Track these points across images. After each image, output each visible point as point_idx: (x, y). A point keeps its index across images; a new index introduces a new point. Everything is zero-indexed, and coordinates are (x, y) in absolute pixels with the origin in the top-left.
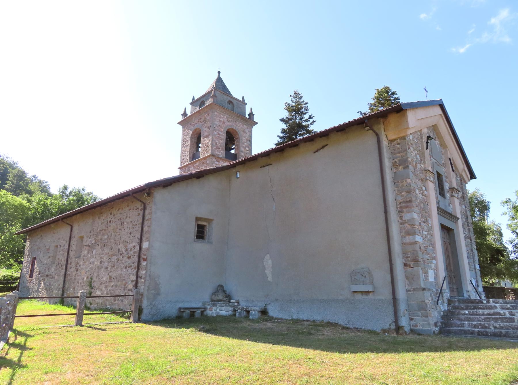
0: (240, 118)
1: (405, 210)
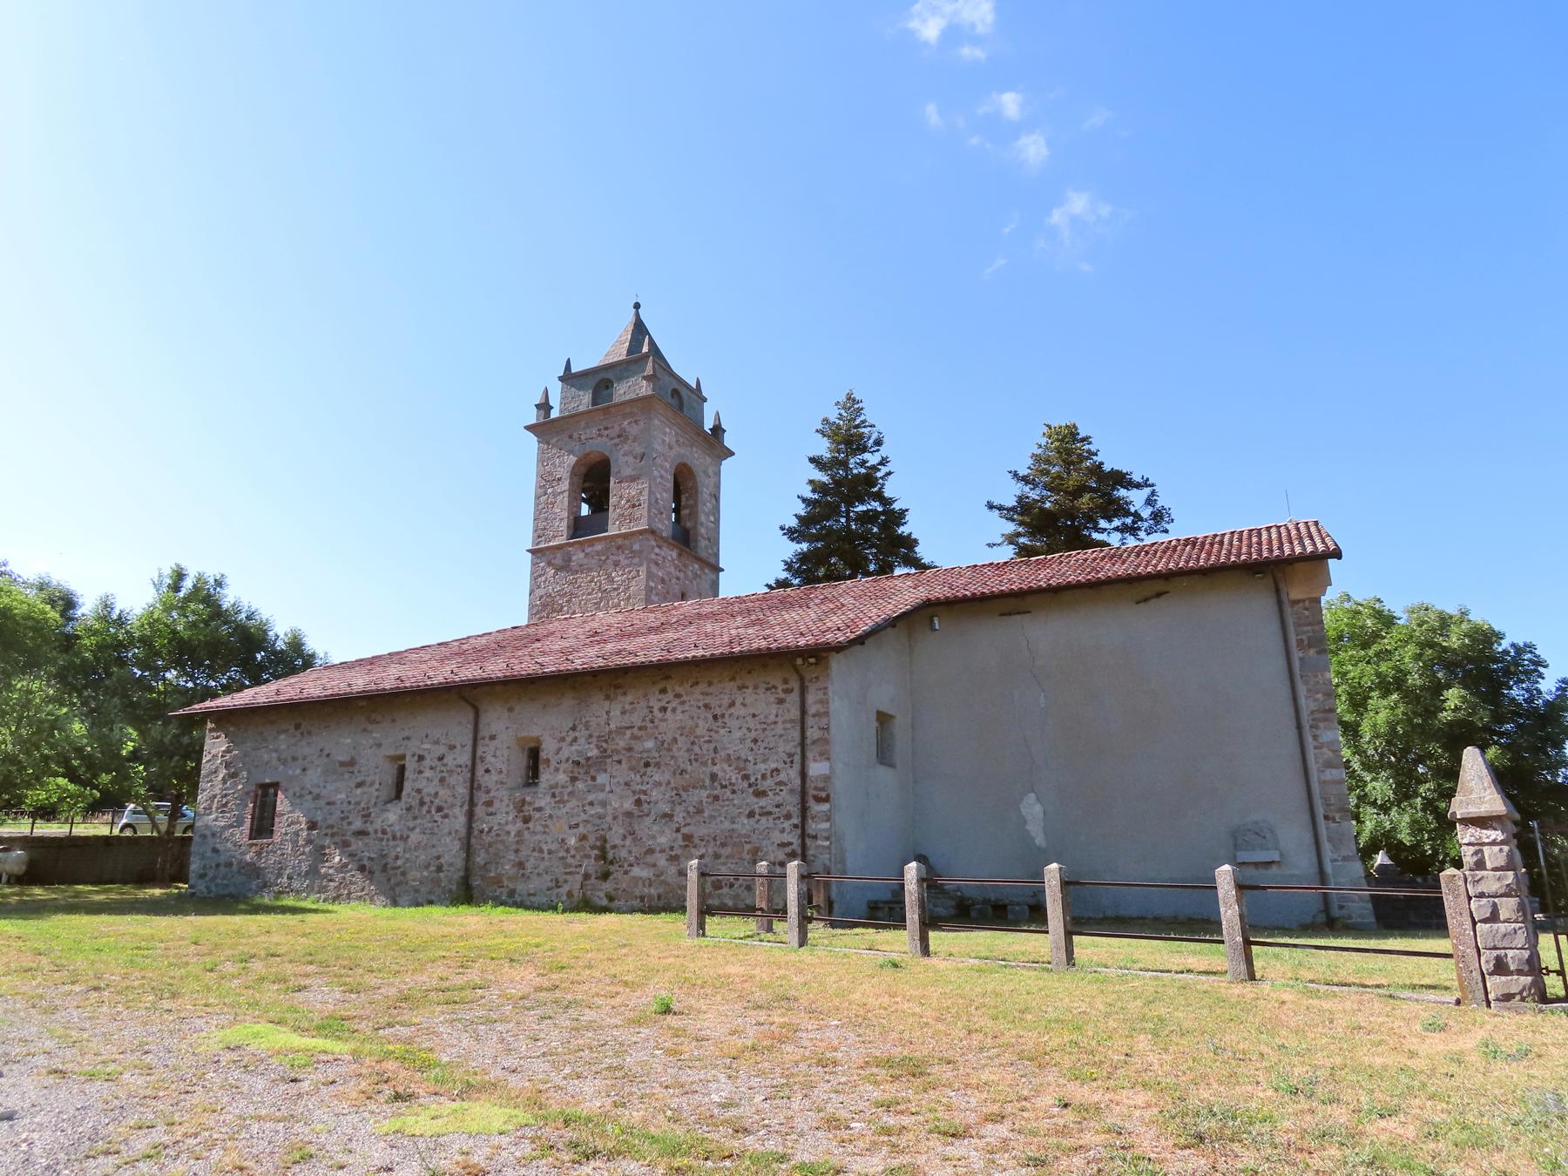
1: (1321, 725)
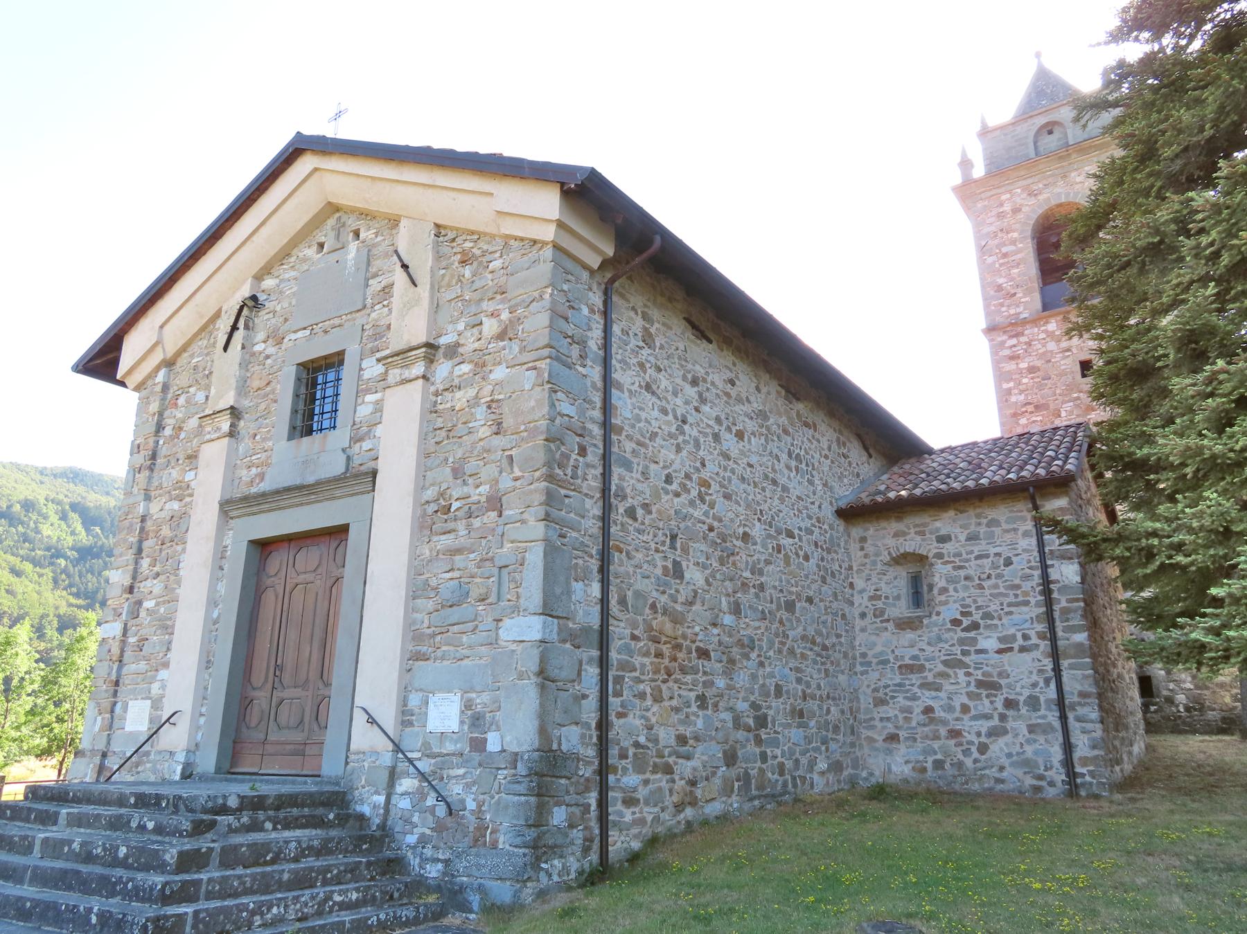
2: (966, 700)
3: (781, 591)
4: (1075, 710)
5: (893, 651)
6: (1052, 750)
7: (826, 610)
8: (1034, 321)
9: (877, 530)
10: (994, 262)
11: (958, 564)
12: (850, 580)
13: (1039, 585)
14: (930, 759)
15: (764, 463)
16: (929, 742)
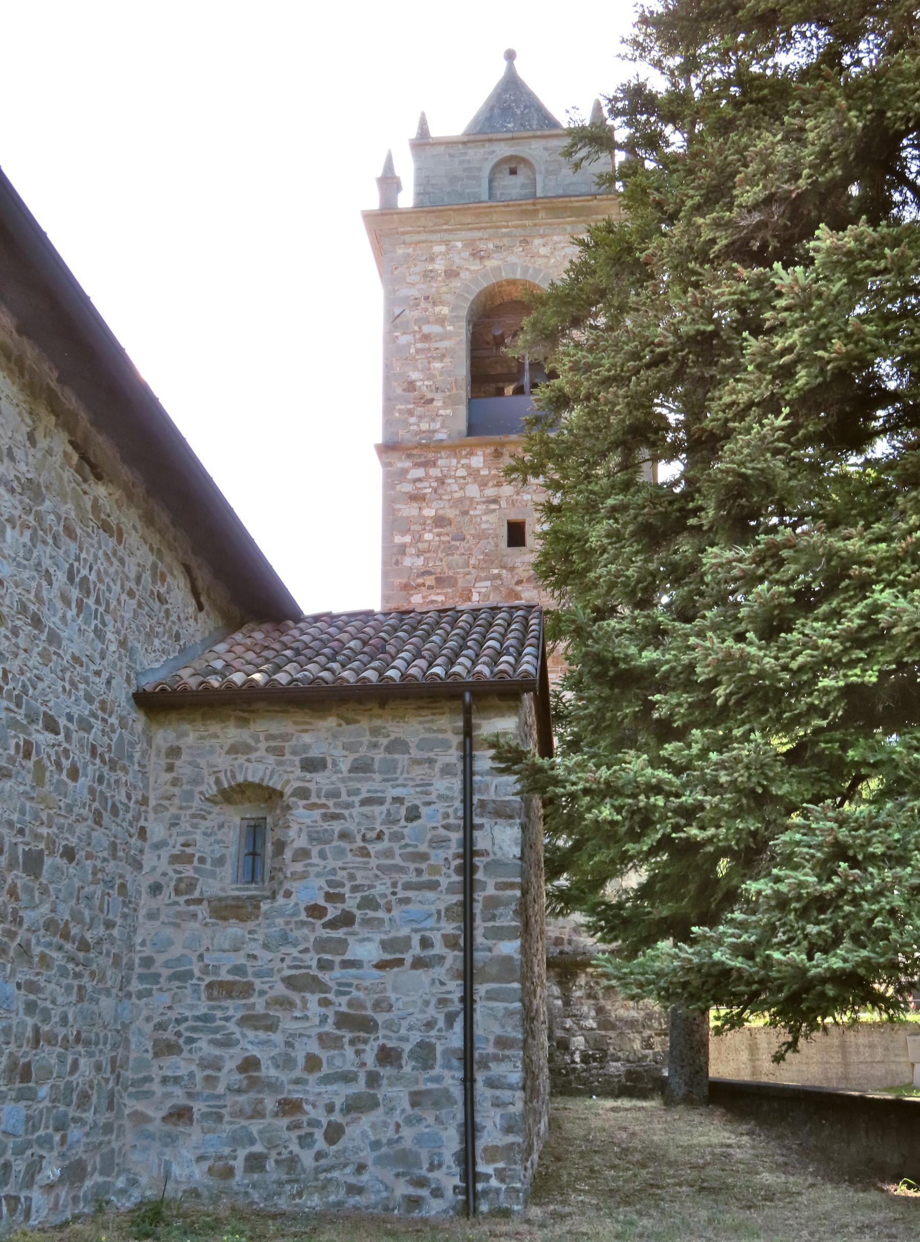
0: (542, 214)
2: (314, 1047)
3: (21, 832)
4: (487, 1068)
5: (201, 957)
6: (445, 1135)
7: (94, 874)
8: (454, 448)
9: (202, 738)
10: (408, 345)
11: (333, 810)
12: (142, 823)
13: (457, 856)
14: (242, 1153)
15: (23, 581)
16: (244, 1123)
